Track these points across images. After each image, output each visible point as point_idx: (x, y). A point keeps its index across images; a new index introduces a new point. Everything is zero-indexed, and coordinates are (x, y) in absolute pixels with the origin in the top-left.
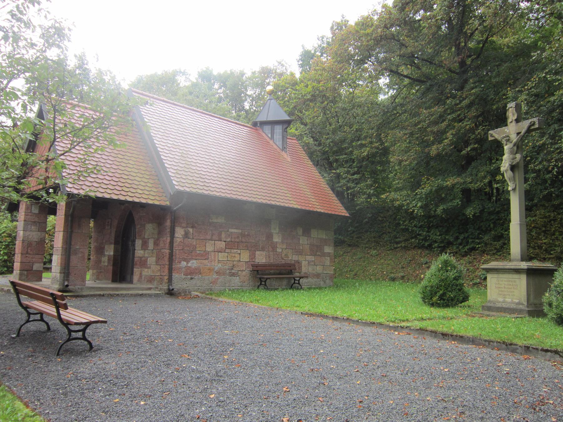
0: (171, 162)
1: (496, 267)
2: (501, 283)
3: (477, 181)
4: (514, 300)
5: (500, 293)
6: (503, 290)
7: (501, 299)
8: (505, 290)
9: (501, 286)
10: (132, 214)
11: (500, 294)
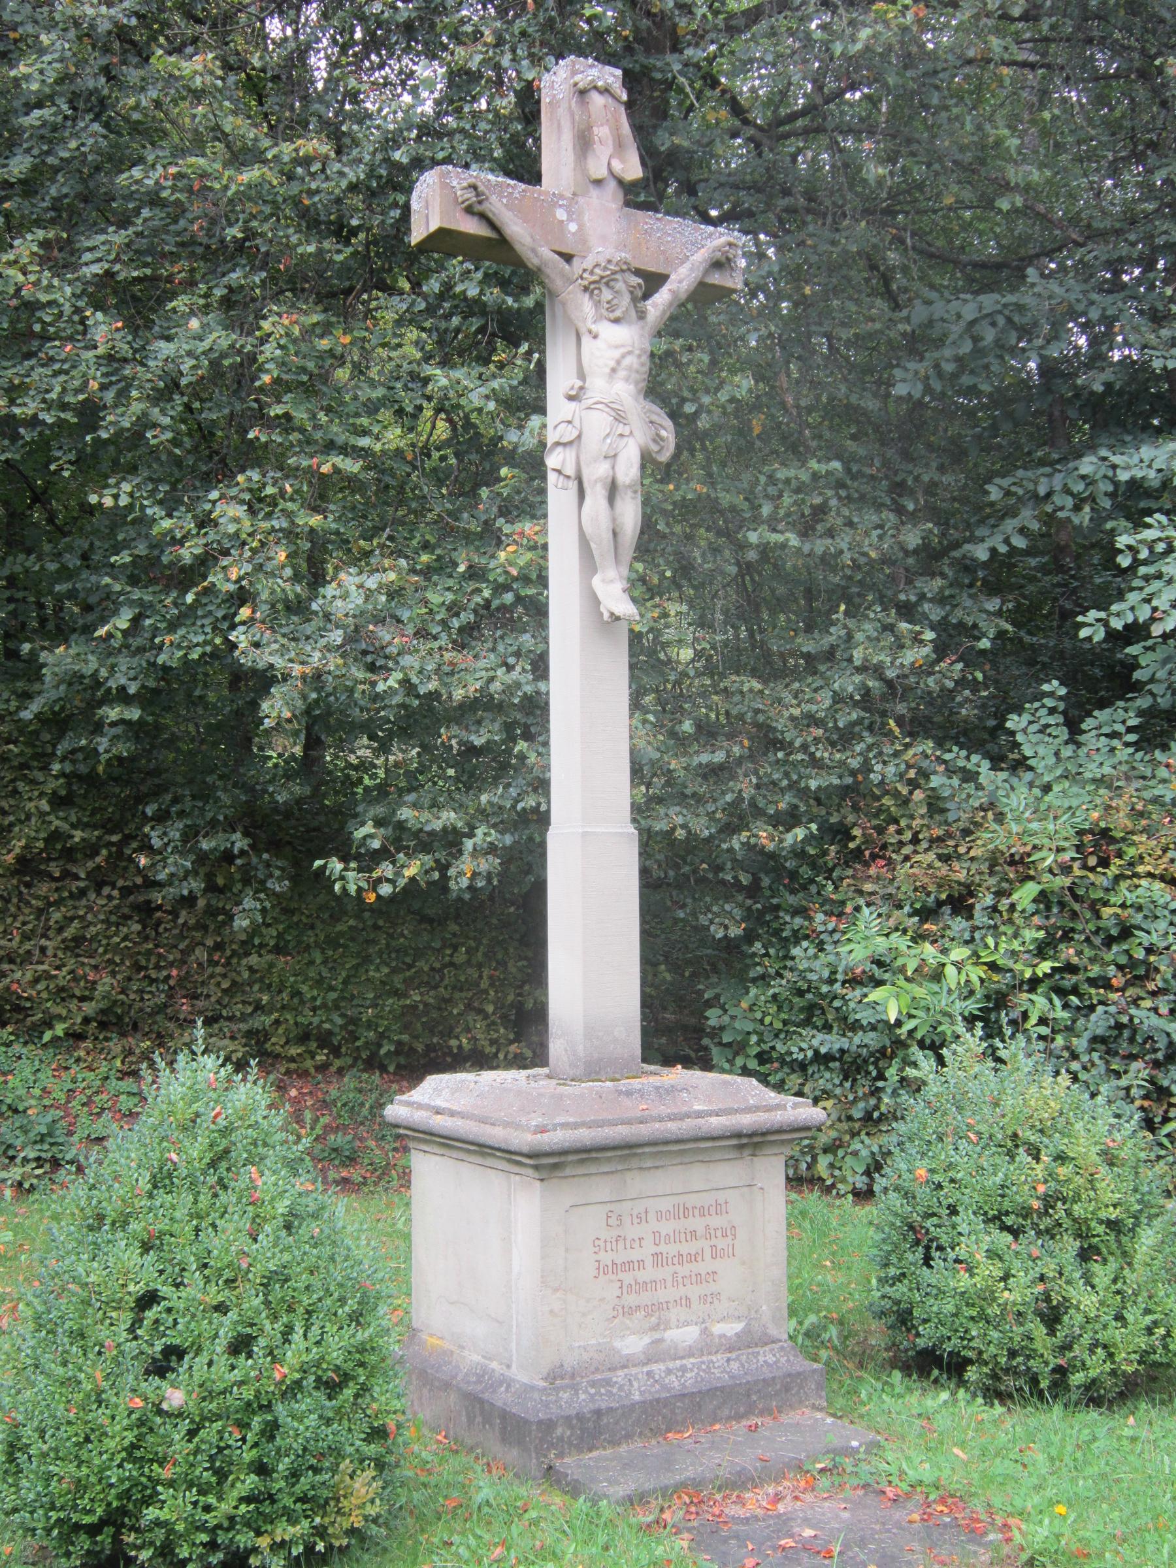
2: (632, 1231)
4: (718, 1329)
5: (631, 1300)
6: (643, 1276)
7: (633, 1344)
8: (665, 1273)
9: (635, 1255)
10: (543, 313)
11: (631, 1311)
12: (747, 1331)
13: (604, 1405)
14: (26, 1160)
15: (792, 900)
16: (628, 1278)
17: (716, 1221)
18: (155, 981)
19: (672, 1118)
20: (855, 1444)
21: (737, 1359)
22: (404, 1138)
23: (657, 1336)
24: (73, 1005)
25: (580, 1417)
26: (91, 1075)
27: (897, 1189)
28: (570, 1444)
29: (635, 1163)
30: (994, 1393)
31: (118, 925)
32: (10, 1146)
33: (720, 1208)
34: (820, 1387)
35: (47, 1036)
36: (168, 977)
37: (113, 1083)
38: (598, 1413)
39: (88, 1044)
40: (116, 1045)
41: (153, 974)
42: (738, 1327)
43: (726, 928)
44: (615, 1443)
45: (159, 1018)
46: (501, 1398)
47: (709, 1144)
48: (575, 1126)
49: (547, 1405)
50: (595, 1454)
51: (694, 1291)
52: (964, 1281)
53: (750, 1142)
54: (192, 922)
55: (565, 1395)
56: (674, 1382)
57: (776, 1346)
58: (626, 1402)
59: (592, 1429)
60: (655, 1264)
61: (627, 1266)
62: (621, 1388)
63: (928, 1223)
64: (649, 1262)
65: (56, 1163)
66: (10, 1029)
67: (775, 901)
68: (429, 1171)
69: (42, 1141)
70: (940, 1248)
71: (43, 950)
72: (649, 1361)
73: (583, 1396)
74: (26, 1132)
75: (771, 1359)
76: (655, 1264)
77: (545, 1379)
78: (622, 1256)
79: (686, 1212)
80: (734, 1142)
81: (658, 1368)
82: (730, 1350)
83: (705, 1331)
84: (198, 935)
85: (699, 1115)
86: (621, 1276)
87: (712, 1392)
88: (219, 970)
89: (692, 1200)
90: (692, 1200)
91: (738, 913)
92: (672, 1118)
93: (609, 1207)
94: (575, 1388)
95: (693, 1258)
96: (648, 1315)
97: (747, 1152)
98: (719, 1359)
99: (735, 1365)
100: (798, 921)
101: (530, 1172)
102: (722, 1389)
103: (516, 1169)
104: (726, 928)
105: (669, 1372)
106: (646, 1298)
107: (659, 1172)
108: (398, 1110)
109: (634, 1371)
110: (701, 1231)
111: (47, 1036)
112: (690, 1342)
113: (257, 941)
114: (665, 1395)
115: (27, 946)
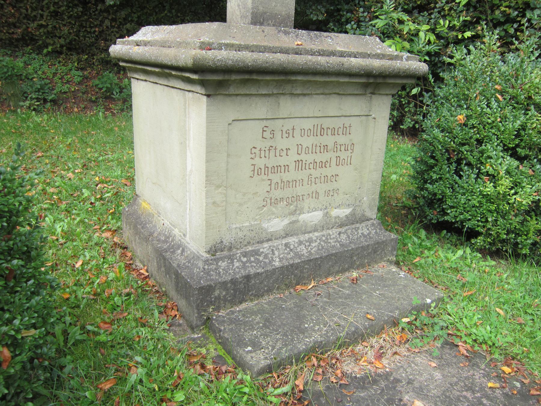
0: (204, 106)
1: (248, 58)
2: (282, 143)
3: (104, 224)
4: (335, 212)
5: (277, 194)
6: (286, 176)
7: (276, 224)
8: (303, 175)
9: (282, 161)
11: (276, 202)
12: (353, 214)
13: (252, 271)
14: (32, 99)
15: (346, 7)
16: (276, 178)
17: (342, 139)
18: (90, 32)
19: (322, 53)
20: (429, 301)
21: (346, 232)
22: (123, 68)
23: (294, 218)
24: (56, 40)
25: (234, 282)
26: (64, 68)
27: (438, 126)
28: (225, 300)
29: (288, 88)
30: (494, 252)
31: (73, 8)
32: (25, 93)
33: (346, 130)
34: (394, 249)
35: (45, 51)
36: (95, 31)
37: (73, 72)
38: (248, 277)
39: (63, 56)
40: (75, 57)
41: (89, 30)
42: (348, 211)
43: (318, 15)
44: (258, 296)
45: (93, 48)
46: (178, 259)
47: (346, 80)
48: (239, 48)
49: (207, 273)
50: (244, 306)
51: (321, 188)
52: (489, 188)
53: (371, 82)
54: (103, 8)
55: (223, 264)
56: (303, 250)
57: (369, 223)
58: (269, 268)
59: (242, 289)
60: (297, 168)
61: (276, 169)
62: (266, 257)
63: (463, 149)
64: (292, 166)
65: (45, 101)
66: (30, 47)
67: (339, 7)
68: (144, 93)
69: (39, 91)
70: (469, 164)
71: (42, 16)
72: (287, 235)
73: (237, 264)
74: (32, 87)
75: (366, 232)
76: (297, 168)
77: (208, 252)
78: (272, 162)
79: (322, 131)
80: (363, 80)
81: (292, 240)
82: (341, 226)
83: (326, 215)
84: (105, 14)
85: (342, 54)
86: (271, 176)
87: (329, 257)
88: (115, 29)
89: (327, 123)
90: (327, 123)
91: (323, 10)
92: (322, 53)
93: (265, 123)
94: (231, 258)
95: (323, 165)
96: (289, 204)
97: (369, 90)
98: (334, 232)
99: (344, 237)
100: (349, 15)
101: (198, 88)
102: (335, 255)
103: (189, 87)
104: (318, 15)
105: (300, 243)
106: (288, 192)
107: (306, 99)
108: (119, 48)
109: (275, 243)
110: (331, 146)
111: (45, 51)
112: (316, 222)
113: (130, 19)
114: (297, 261)
115: (34, 13)
